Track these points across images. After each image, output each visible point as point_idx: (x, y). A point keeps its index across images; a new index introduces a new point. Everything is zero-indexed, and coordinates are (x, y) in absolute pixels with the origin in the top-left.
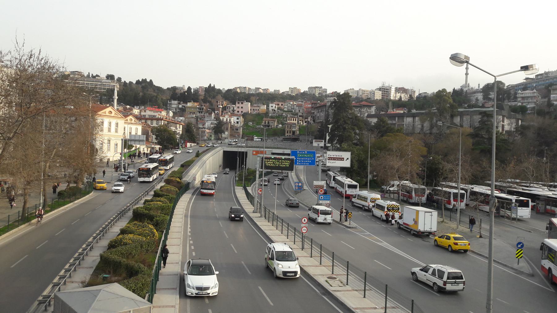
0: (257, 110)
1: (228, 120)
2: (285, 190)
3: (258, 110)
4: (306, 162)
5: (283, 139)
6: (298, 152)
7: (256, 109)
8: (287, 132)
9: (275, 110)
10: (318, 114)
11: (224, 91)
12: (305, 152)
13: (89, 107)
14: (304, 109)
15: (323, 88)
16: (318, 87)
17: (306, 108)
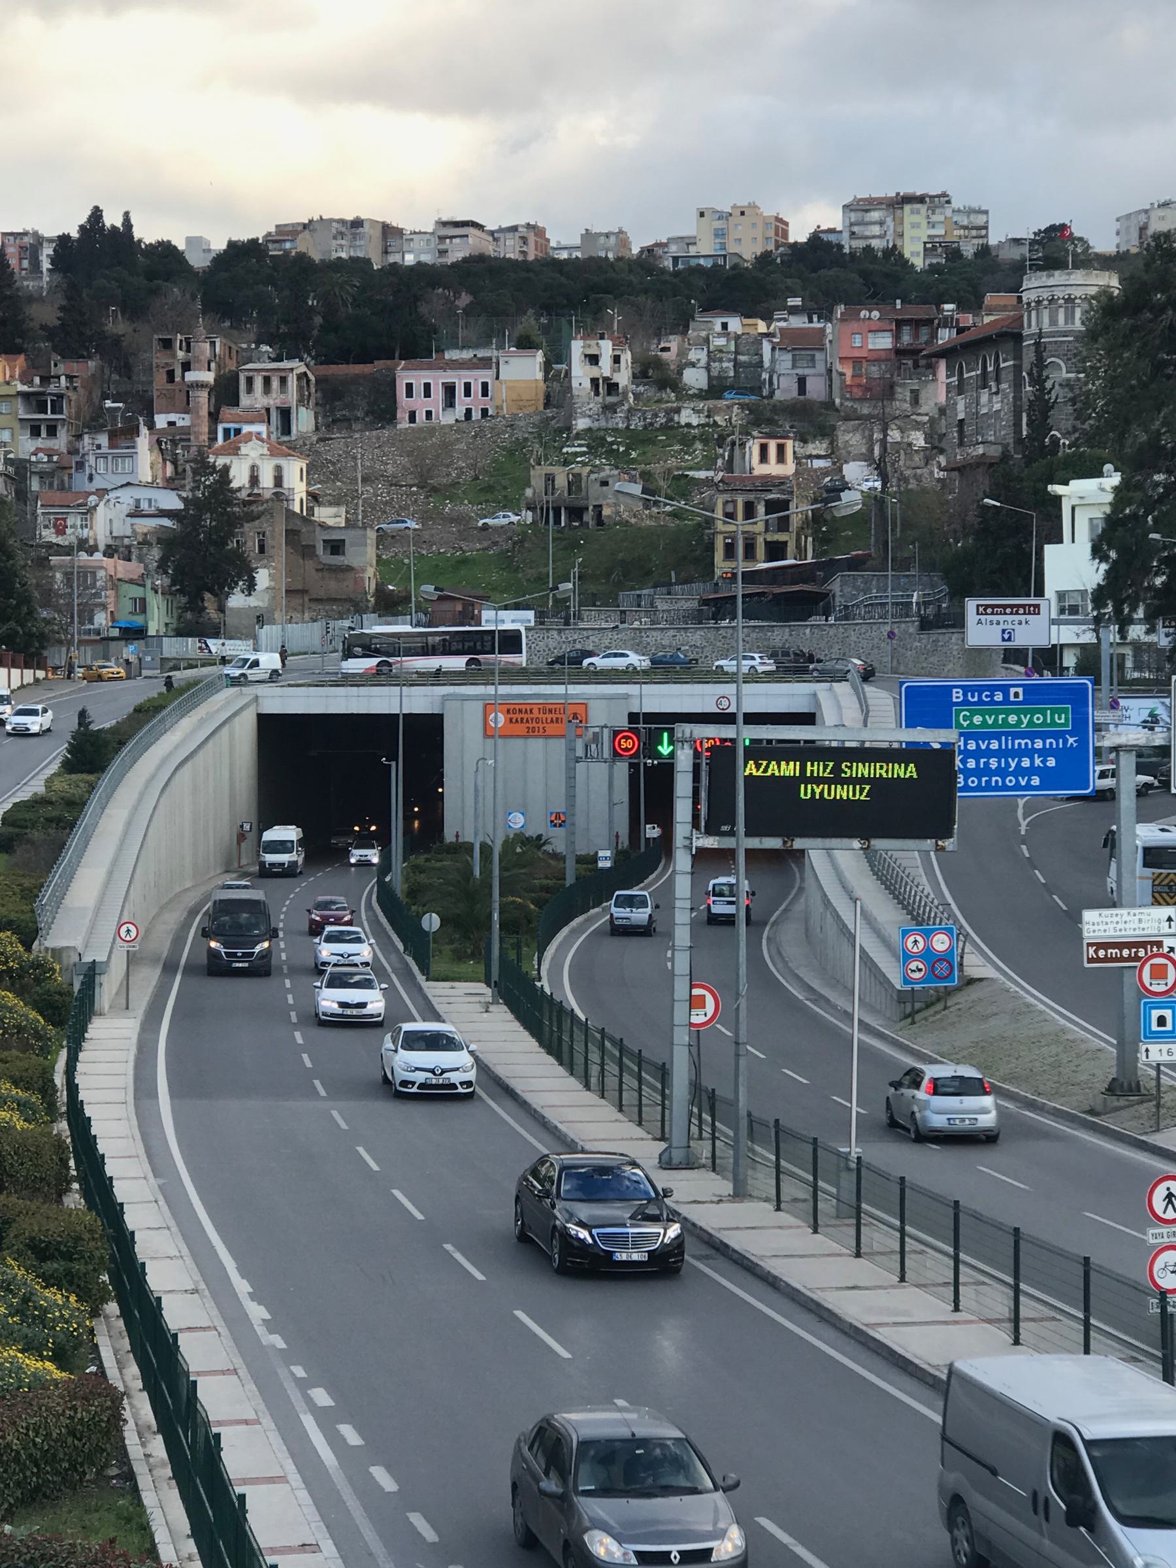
0: (476, 389)
1: (267, 480)
2: (811, 989)
3: (485, 393)
4: (1020, 771)
5: (705, 602)
6: (957, 696)
7: (427, 386)
8: (730, 552)
9: (612, 387)
10: (961, 406)
11: (198, 261)
12: (1006, 695)
14: (838, 367)
15: (956, 204)
16: (921, 200)
17: (857, 362)
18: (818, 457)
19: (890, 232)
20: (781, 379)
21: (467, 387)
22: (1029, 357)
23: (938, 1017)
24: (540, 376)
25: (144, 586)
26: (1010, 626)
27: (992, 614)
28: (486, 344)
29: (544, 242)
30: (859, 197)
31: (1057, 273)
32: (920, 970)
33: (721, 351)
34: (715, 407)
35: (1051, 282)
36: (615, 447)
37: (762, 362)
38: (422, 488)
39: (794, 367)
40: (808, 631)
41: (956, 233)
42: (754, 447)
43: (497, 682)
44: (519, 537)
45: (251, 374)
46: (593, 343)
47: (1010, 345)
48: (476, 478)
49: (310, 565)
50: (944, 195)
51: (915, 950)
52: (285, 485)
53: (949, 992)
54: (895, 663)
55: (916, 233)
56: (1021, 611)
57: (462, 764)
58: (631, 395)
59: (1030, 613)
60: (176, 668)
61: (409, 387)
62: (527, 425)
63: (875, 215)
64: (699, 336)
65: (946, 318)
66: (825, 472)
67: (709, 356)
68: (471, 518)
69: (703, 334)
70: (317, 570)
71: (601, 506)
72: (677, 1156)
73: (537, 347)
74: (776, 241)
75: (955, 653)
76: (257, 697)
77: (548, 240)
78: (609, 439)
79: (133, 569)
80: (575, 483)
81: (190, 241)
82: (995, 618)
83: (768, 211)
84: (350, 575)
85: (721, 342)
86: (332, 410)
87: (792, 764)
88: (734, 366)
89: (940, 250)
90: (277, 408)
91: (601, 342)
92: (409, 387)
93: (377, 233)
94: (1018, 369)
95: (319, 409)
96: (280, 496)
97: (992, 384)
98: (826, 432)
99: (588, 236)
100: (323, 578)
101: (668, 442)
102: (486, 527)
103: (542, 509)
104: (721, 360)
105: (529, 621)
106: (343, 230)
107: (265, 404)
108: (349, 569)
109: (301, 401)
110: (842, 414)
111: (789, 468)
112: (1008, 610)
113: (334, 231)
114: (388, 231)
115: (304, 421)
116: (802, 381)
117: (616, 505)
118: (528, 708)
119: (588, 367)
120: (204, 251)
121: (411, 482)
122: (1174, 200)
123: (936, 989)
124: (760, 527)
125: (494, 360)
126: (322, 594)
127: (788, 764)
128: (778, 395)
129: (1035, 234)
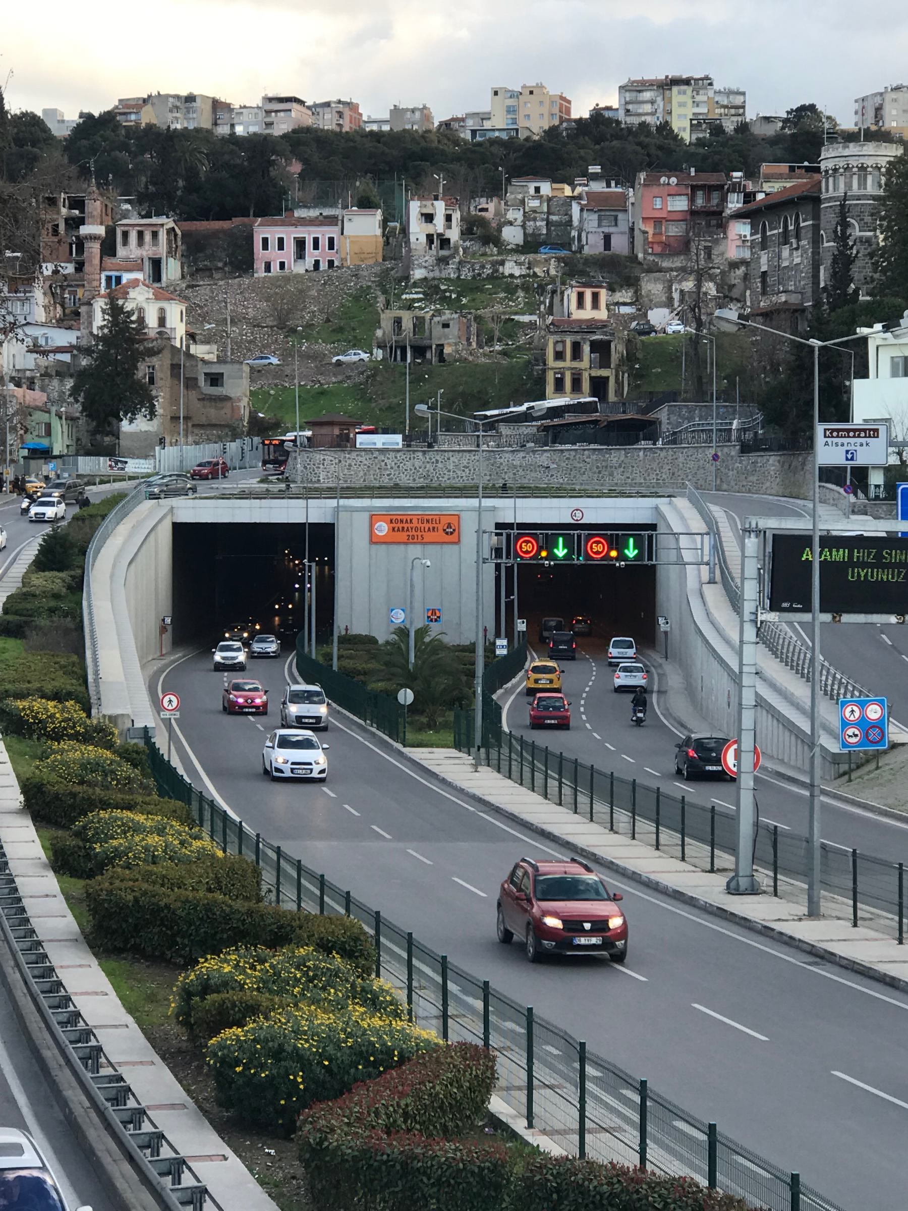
0: (324, 243)
3: (331, 247)
7: (281, 241)
9: (445, 242)
10: (764, 259)
13: (466, 359)
16: (687, 82)
18: (625, 304)
19: (660, 110)
20: (590, 236)
21: (316, 241)
22: (829, 219)
23: (872, 775)
24: (379, 232)
25: (49, 412)
26: (853, 448)
27: (838, 437)
28: (333, 205)
29: (358, 117)
30: (632, 79)
31: (851, 145)
32: (856, 736)
33: (535, 212)
34: (535, 259)
35: (846, 152)
36: (448, 294)
37: (571, 221)
38: (281, 329)
39: (599, 226)
40: (641, 453)
41: (718, 111)
42: (571, 295)
43: (339, 496)
44: (373, 372)
45: (126, 229)
46: (429, 203)
47: (809, 208)
48: (328, 320)
49: (193, 395)
50: (707, 78)
51: (852, 718)
52: (168, 325)
53: (878, 755)
54: (718, 482)
55: (682, 111)
56: (863, 434)
57: (351, 568)
58: (461, 249)
59: (870, 437)
60: (89, 483)
61: (265, 241)
62: (369, 275)
63: (647, 95)
64: (515, 198)
65: (734, 184)
66: (633, 318)
67: (524, 216)
68: (325, 355)
69: (520, 196)
70: (199, 399)
71: (442, 345)
72: (744, 883)
73: (375, 206)
74: (561, 117)
75: (772, 473)
76: (172, 508)
77: (361, 115)
78: (443, 287)
79: (36, 397)
80: (419, 324)
81: (45, 111)
82: (840, 440)
83: (553, 89)
84: (229, 404)
85: (535, 203)
86: (195, 261)
87: (841, 551)
88: (547, 225)
89: (704, 126)
90: (149, 258)
91: (435, 203)
92: (265, 241)
93: (208, 107)
94: (816, 228)
95: (184, 260)
96: (164, 335)
97: (794, 241)
98: (632, 282)
99: (396, 111)
100: (204, 407)
101: (493, 290)
102: (339, 363)
103: (391, 348)
104: (535, 219)
105: (398, 444)
106: (179, 104)
107: (139, 255)
108: (227, 398)
109: (171, 253)
110: (645, 267)
111: (602, 314)
112: (851, 434)
113: (170, 105)
114: (217, 105)
115: (172, 270)
116: (607, 238)
117: (456, 344)
118: (409, 518)
119: (424, 225)
120: (59, 121)
121: (271, 324)
122: (904, 84)
123: (865, 753)
124: (585, 363)
125: (340, 218)
126: (203, 420)
127: (838, 551)
128: (587, 250)
129: (788, 112)
